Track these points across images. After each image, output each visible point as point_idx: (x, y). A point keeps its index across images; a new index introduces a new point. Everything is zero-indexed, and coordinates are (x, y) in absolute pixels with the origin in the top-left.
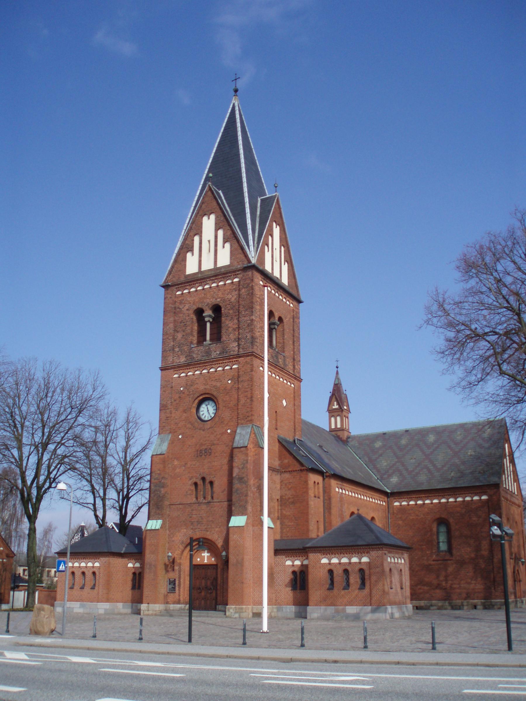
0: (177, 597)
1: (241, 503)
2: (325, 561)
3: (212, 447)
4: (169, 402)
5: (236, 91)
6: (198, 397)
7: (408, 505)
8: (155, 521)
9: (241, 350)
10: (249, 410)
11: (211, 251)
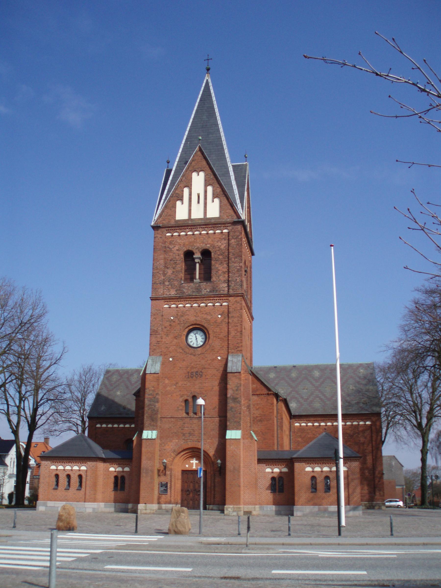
0: (169, 498)
1: (235, 420)
2: (309, 469)
3: (203, 371)
4: (160, 328)
5: (208, 70)
6: (189, 326)
7: (307, 426)
8: (150, 432)
9: (231, 290)
10: (239, 341)
11: (198, 202)
